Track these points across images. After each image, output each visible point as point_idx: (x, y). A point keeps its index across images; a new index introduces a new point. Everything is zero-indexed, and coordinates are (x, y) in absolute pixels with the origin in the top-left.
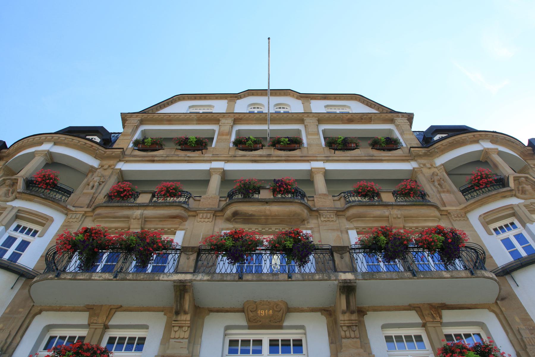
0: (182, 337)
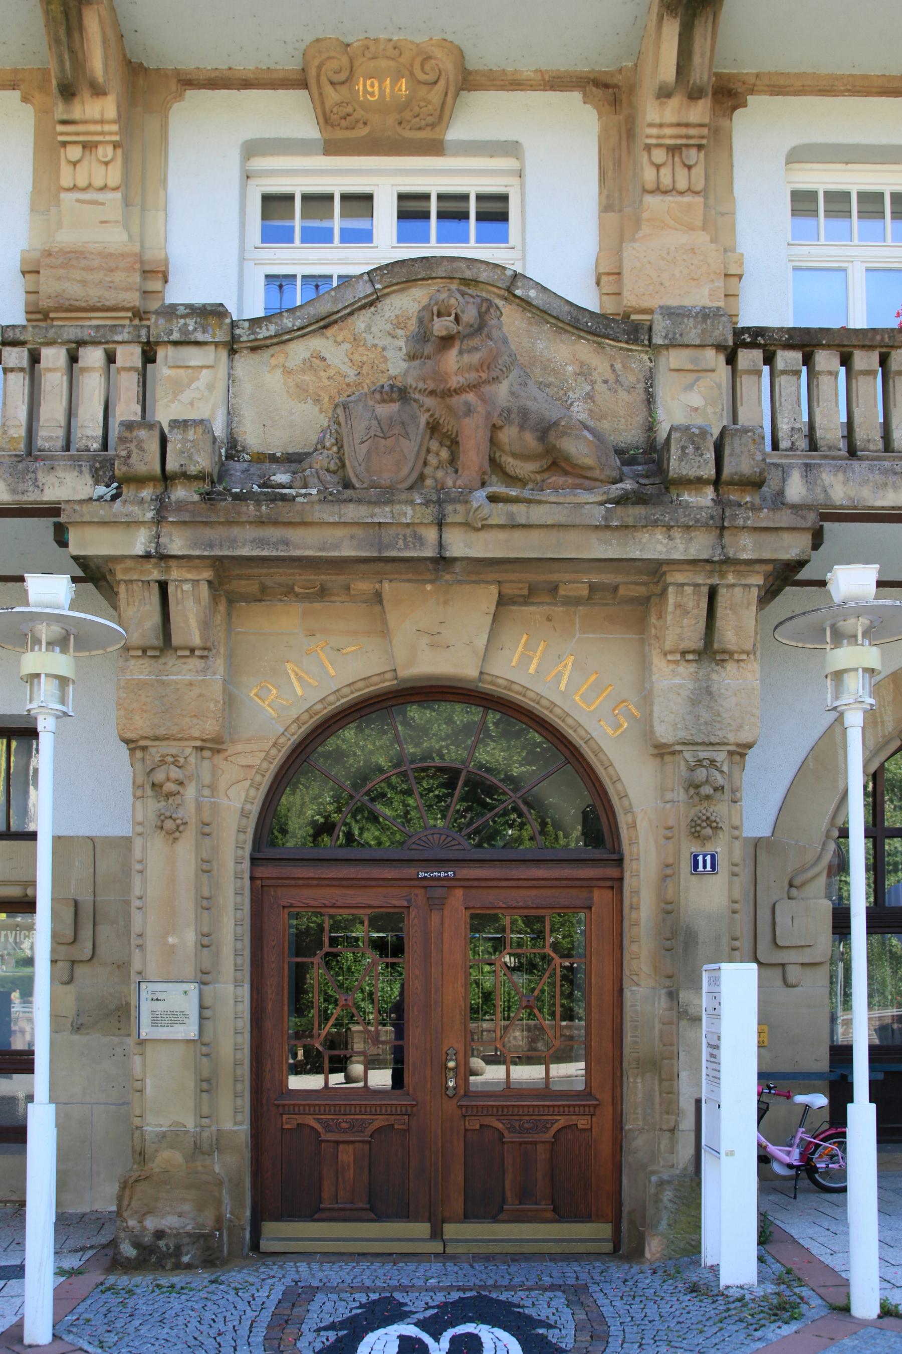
0: (98, 182)
